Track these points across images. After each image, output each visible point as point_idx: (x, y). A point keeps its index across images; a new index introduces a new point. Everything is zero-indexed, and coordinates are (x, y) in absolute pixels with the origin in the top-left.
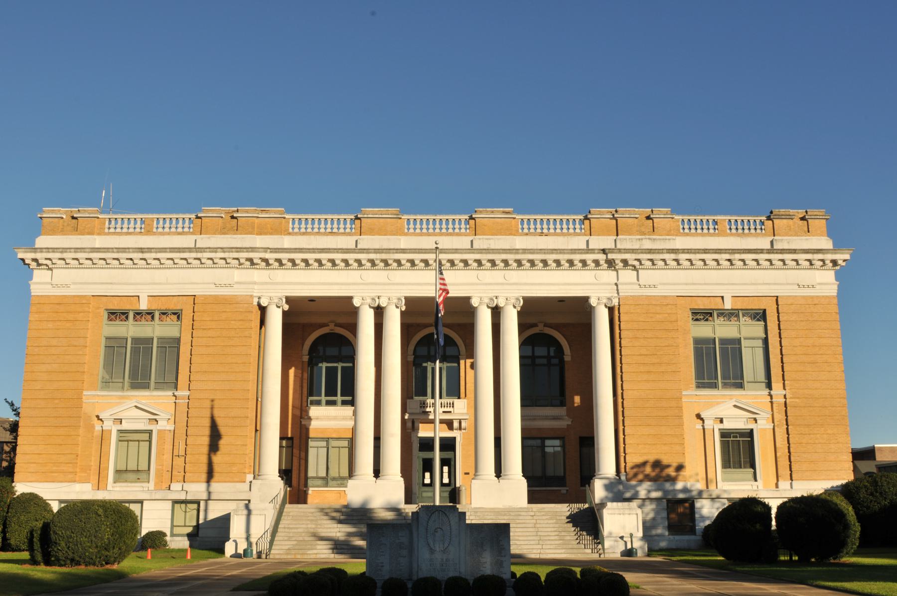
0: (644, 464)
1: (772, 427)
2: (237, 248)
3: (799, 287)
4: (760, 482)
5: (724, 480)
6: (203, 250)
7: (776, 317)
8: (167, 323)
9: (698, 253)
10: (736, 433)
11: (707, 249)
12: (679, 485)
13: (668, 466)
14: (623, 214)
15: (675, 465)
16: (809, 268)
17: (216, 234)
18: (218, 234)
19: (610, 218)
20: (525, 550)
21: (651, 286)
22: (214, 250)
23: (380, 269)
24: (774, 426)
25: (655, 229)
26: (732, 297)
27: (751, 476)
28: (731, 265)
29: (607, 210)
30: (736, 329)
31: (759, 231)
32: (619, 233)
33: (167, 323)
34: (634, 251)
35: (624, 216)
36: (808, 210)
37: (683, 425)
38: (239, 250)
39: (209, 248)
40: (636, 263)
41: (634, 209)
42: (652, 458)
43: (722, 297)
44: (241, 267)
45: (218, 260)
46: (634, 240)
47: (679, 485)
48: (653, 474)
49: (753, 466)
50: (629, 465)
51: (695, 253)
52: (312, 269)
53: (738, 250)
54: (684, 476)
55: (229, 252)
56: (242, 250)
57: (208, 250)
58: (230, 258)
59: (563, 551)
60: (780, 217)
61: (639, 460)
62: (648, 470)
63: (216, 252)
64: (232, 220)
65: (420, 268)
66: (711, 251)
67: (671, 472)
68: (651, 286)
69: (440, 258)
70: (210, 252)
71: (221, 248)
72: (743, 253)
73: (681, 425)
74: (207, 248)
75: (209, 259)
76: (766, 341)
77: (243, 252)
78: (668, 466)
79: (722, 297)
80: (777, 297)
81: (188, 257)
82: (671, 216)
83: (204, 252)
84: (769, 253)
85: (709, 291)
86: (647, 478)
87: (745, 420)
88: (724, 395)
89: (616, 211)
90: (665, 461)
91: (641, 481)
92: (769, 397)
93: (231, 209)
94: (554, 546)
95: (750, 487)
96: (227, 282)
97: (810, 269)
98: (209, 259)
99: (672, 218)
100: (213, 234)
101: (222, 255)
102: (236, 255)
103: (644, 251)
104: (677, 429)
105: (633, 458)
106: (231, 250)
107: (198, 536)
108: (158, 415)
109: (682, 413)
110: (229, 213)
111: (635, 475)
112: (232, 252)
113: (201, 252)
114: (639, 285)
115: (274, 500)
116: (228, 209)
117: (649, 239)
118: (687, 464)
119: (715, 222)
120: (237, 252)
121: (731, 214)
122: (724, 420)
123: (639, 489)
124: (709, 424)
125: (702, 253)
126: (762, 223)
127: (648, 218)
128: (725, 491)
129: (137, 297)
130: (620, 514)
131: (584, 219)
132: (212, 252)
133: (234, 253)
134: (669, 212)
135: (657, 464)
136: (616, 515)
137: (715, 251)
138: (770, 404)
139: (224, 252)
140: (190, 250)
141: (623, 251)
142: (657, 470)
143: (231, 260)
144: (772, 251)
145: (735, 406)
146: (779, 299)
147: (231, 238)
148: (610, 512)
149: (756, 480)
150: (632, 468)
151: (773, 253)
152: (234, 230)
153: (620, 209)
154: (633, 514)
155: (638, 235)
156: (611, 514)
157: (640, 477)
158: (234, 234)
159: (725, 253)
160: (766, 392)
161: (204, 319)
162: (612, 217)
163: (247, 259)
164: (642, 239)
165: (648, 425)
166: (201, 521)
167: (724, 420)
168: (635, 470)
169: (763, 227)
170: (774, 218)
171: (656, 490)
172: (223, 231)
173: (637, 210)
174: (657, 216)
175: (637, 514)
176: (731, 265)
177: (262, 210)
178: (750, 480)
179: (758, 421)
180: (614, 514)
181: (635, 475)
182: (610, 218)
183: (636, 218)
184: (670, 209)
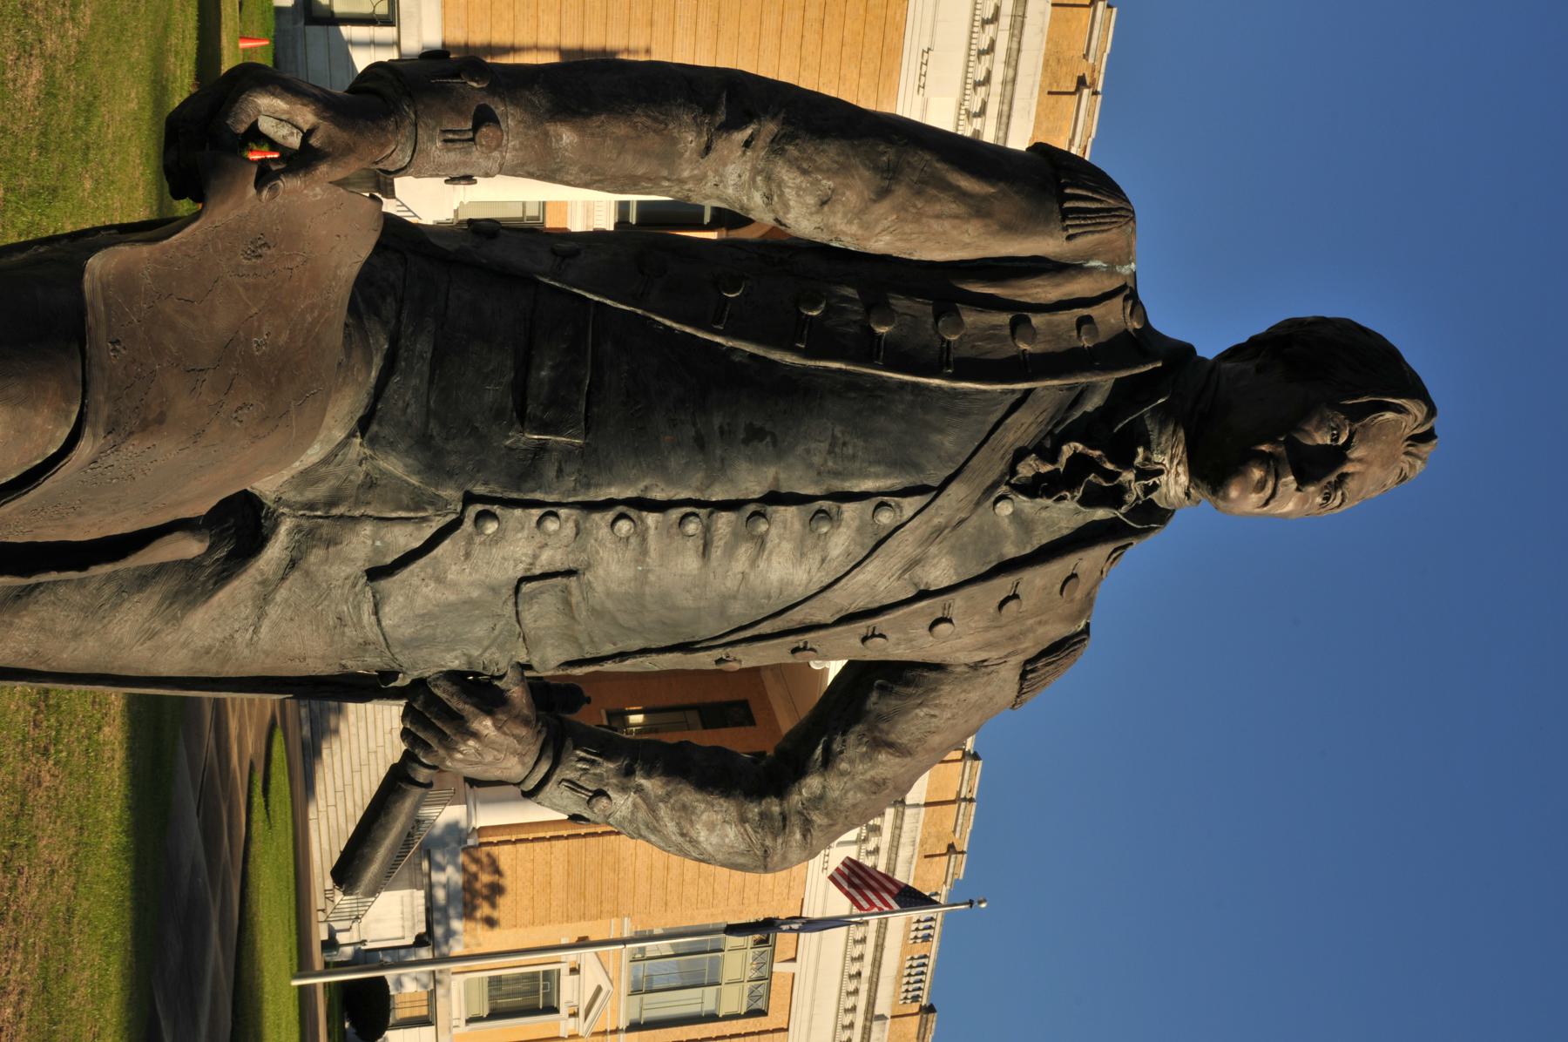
0: (497, 871)
1: (561, 1035)
2: (1009, 117)
3: (923, 51)
4: (464, 1029)
5: (467, 983)
6: (1016, 32)
7: (753, 1030)
8: (748, 967)
9: (878, 937)
10: (552, 989)
11: (882, 949)
12: (457, 925)
13: (493, 905)
14: (964, 815)
15: (495, 914)
16: (973, 47)
17: (1047, 43)
18: (1047, 49)
19: (959, 793)
20: (322, 787)
21: (923, 78)
22: (1013, 60)
23: (975, 9)
24: (563, 1038)
25: (1055, 97)
26: (794, 974)
27: (476, 1012)
28: (983, 19)
29: (976, 785)
30: (737, 976)
31: (913, 935)
32: (931, 808)
33: (748, 967)
34: (894, 849)
35: (960, 817)
36: (965, 855)
37: (567, 921)
38: (1004, 119)
39: (1019, 50)
40: (871, 846)
41: (970, 828)
42: (507, 882)
43: (794, 960)
44: (963, 112)
45: (987, 65)
46: (913, 834)
47: (457, 925)
48: (478, 886)
49: (495, 1014)
50: (495, 850)
51: (878, 931)
52: (960, 114)
53: (876, 990)
54: (475, 929)
55: (1003, 95)
56: (1003, 127)
57: (1015, 46)
58: (992, 62)
59: (326, 846)
60: (923, 1026)
61: (504, 863)
62: (485, 878)
63: (1007, 63)
64: (1075, 80)
65: (975, 35)
66: (878, 954)
67: (484, 910)
68: (923, 78)
69: (871, 922)
70: (1009, 49)
71: (1014, 80)
72: (869, 996)
73: (569, 919)
74: (1019, 43)
75: (989, 73)
76: (712, 1018)
77: (998, 129)
78: (493, 905)
79: (794, 960)
80: (787, 1030)
81: (996, 58)
82: (949, 880)
83: (1012, 36)
84: (867, 1012)
85: (807, 943)
86: (471, 878)
87: (576, 1003)
88: (620, 971)
89: (1095, 93)
90: (503, 901)
91: (464, 869)
92: (614, 1028)
93: (1102, 77)
94: (335, 825)
95: (455, 1014)
96: (929, 81)
97: (966, 78)
98: (989, 73)
99: (945, 882)
100: (1048, 36)
101: (997, 78)
102: (993, 110)
103: (892, 862)
104: (560, 914)
105: (505, 855)
106: (1006, 101)
107: (306, 24)
108: (587, 820)
109: (590, 920)
110: (1093, 71)
111: (477, 861)
112: (1002, 102)
113: (1012, 27)
114: (929, 49)
115: (405, 209)
116: (1103, 71)
117: (912, 856)
118: (497, 931)
119: (926, 938)
120: (1000, 115)
121: (937, 961)
122: (576, 977)
123: (450, 870)
124: (571, 956)
125: (877, 941)
126: (916, 999)
127: (1081, 82)
128: (449, 990)
129: (791, 954)
130: (402, 913)
131: (964, 750)
132: (1009, 56)
133: (997, 105)
134: (956, 877)
135: (496, 890)
136: (400, 908)
137: (878, 959)
138: (603, 1029)
139: (1004, 83)
140: (871, 1003)
141: (897, 832)
142: (485, 891)
143: (983, 96)
144: (871, 1016)
145: (599, 989)
146: (782, 1034)
147: (1034, 82)
148: (407, 900)
149: (470, 1021)
150: (489, 855)
151: (866, 1019)
152: (1051, 85)
153: (974, 808)
154: (404, 931)
155: (923, 834)
156: (402, 901)
157: (473, 868)
158: (1041, 86)
159: (872, 972)
160: (623, 1025)
161: (848, 22)
162: (962, 796)
163: (992, 44)
164: (914, 845)
165: (568, 874)
166: (347, 31)
167: (576, 977)
168: (485, 860)
169: (909, 1001)
170: (922, 1017)
171: (449, 897)
172: (1053, 60)
173: (968, 830)
174: (952, 864)
175: (403, 938)
176: (983, 19)
177: (1086, 147)
178: (468, 1012)
179: (573, 1019)
180: (402, 905)
181: (477, 861)
182: (959, 793)
183: (954, 831)
184: (961, 877)
